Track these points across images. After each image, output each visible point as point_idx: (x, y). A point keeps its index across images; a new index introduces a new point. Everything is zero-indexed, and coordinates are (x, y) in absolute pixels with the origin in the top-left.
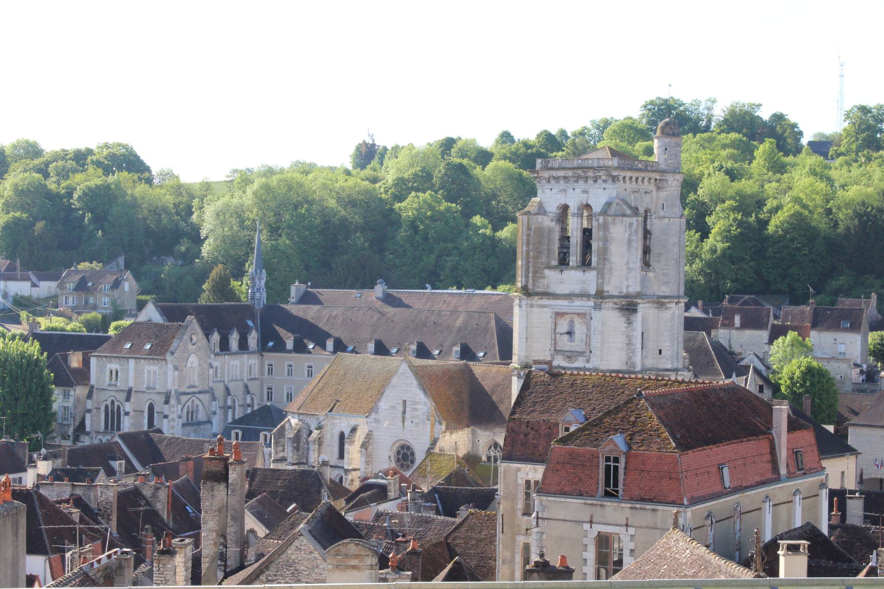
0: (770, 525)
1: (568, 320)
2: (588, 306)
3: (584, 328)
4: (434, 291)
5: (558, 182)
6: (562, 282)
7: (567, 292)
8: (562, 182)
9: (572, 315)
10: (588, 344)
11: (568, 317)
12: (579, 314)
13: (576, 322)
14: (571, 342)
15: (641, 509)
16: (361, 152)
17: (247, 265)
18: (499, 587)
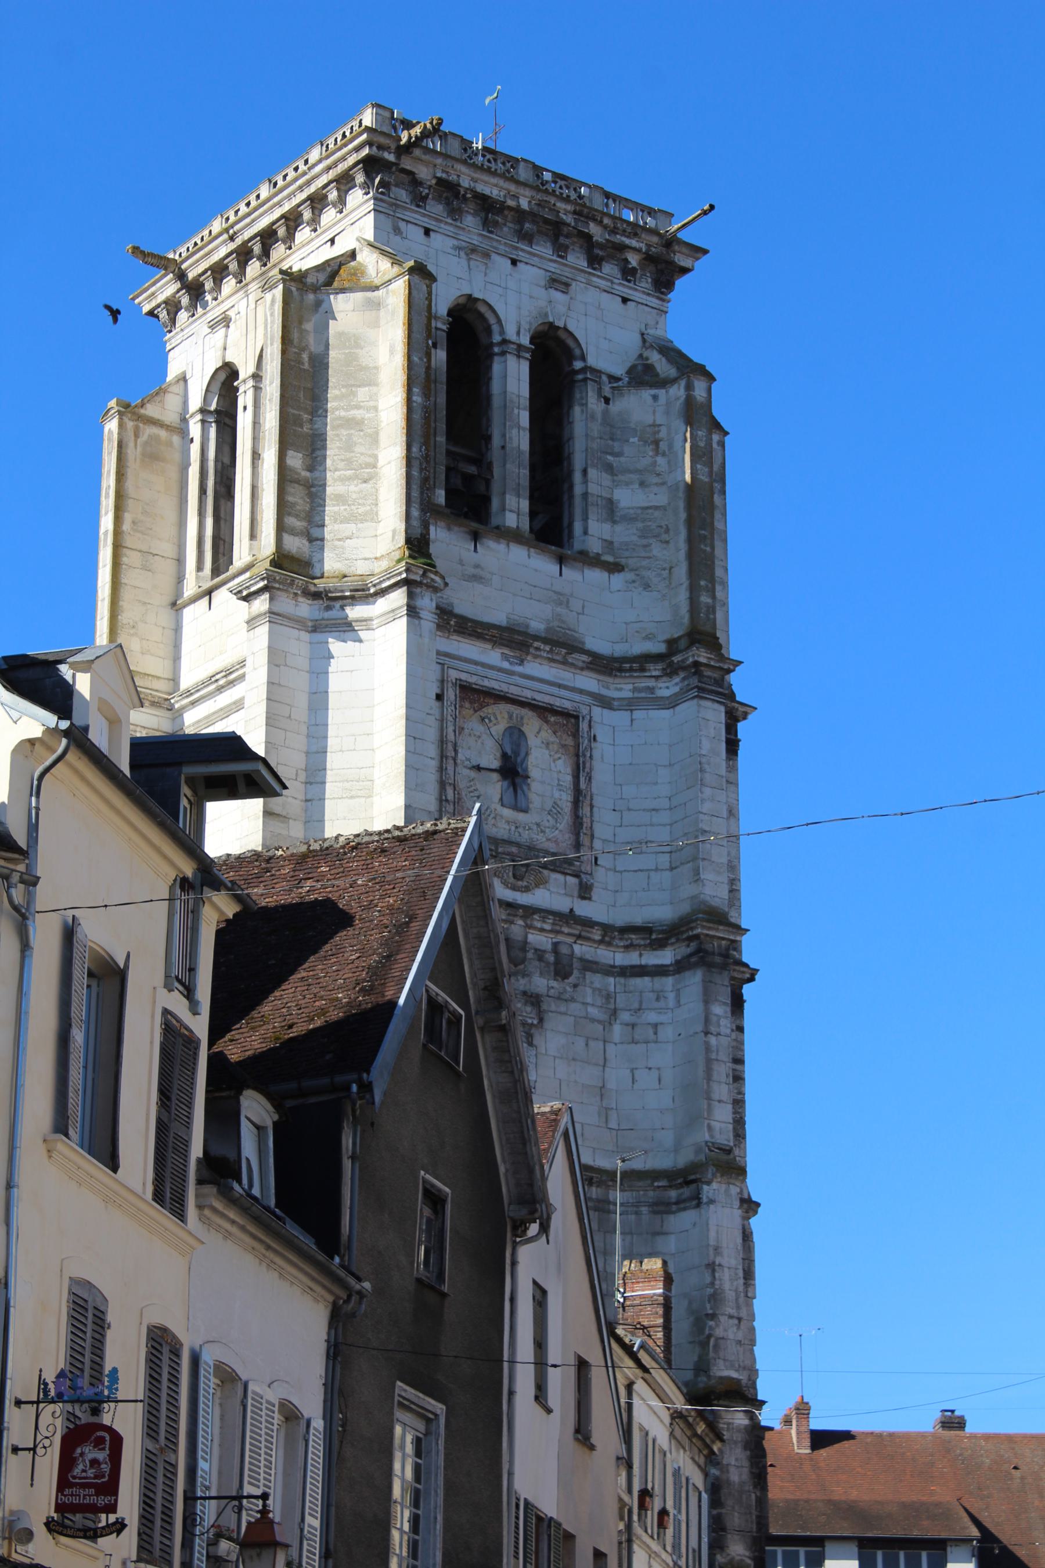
0: (707, 1562)
1: (499, 728)
2: (581, 692)
3: (563, 768)
5: (455, 213)
7: (499, 617)
8: (470, 221)
11: (501, 715)
12: (544, 711)
14: (516, 808)
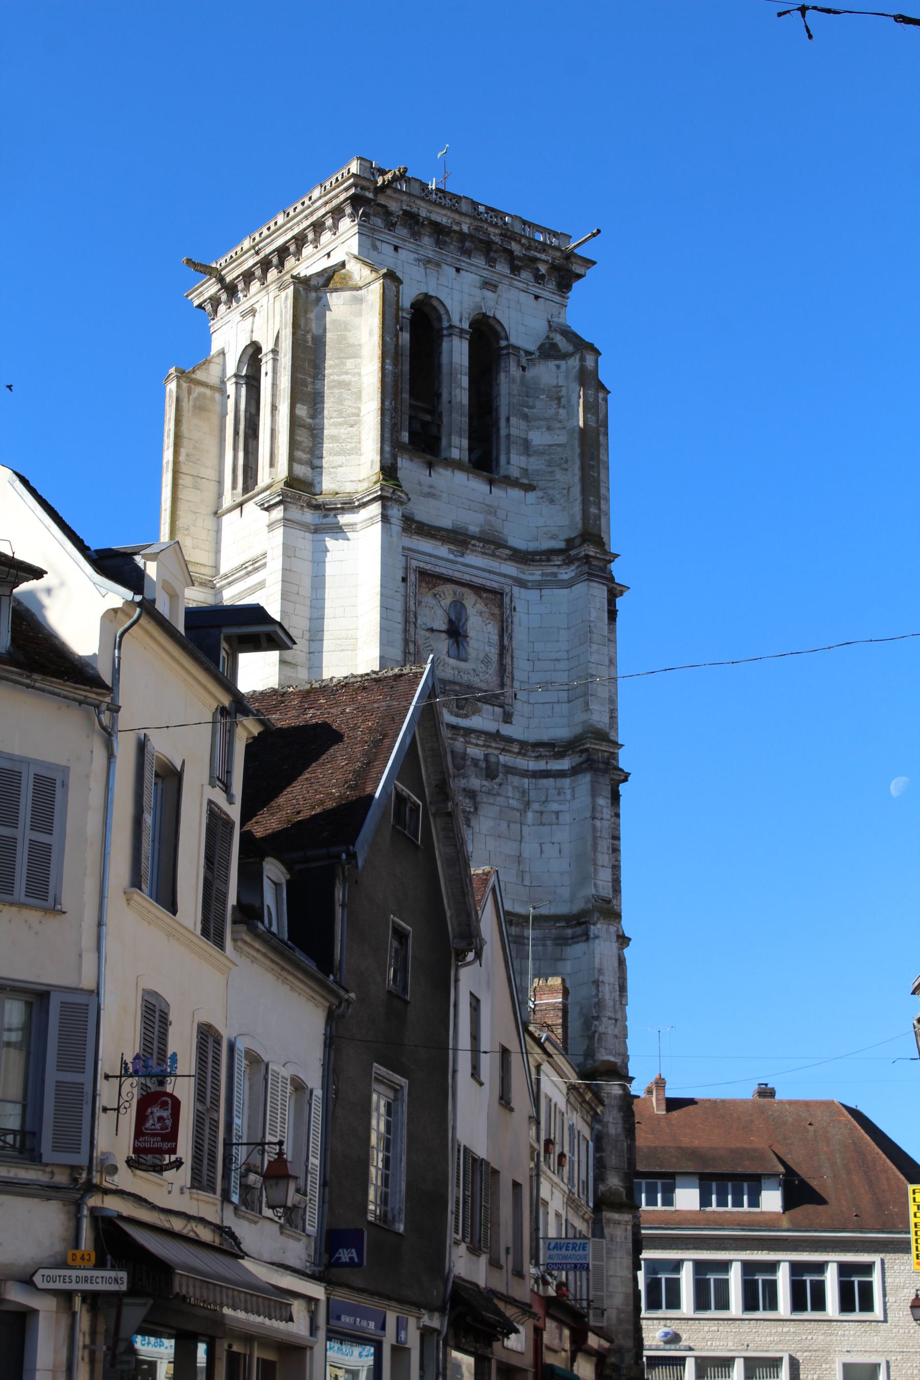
1: (447, 602)
2: (505, 576)
3: (492, 630)
4: (185, 1147)
7: (446, 522)
9: (459, 589)
11: (448, 593)
12: (478, 589)
16: (86, 666)
17: (243, 1170)
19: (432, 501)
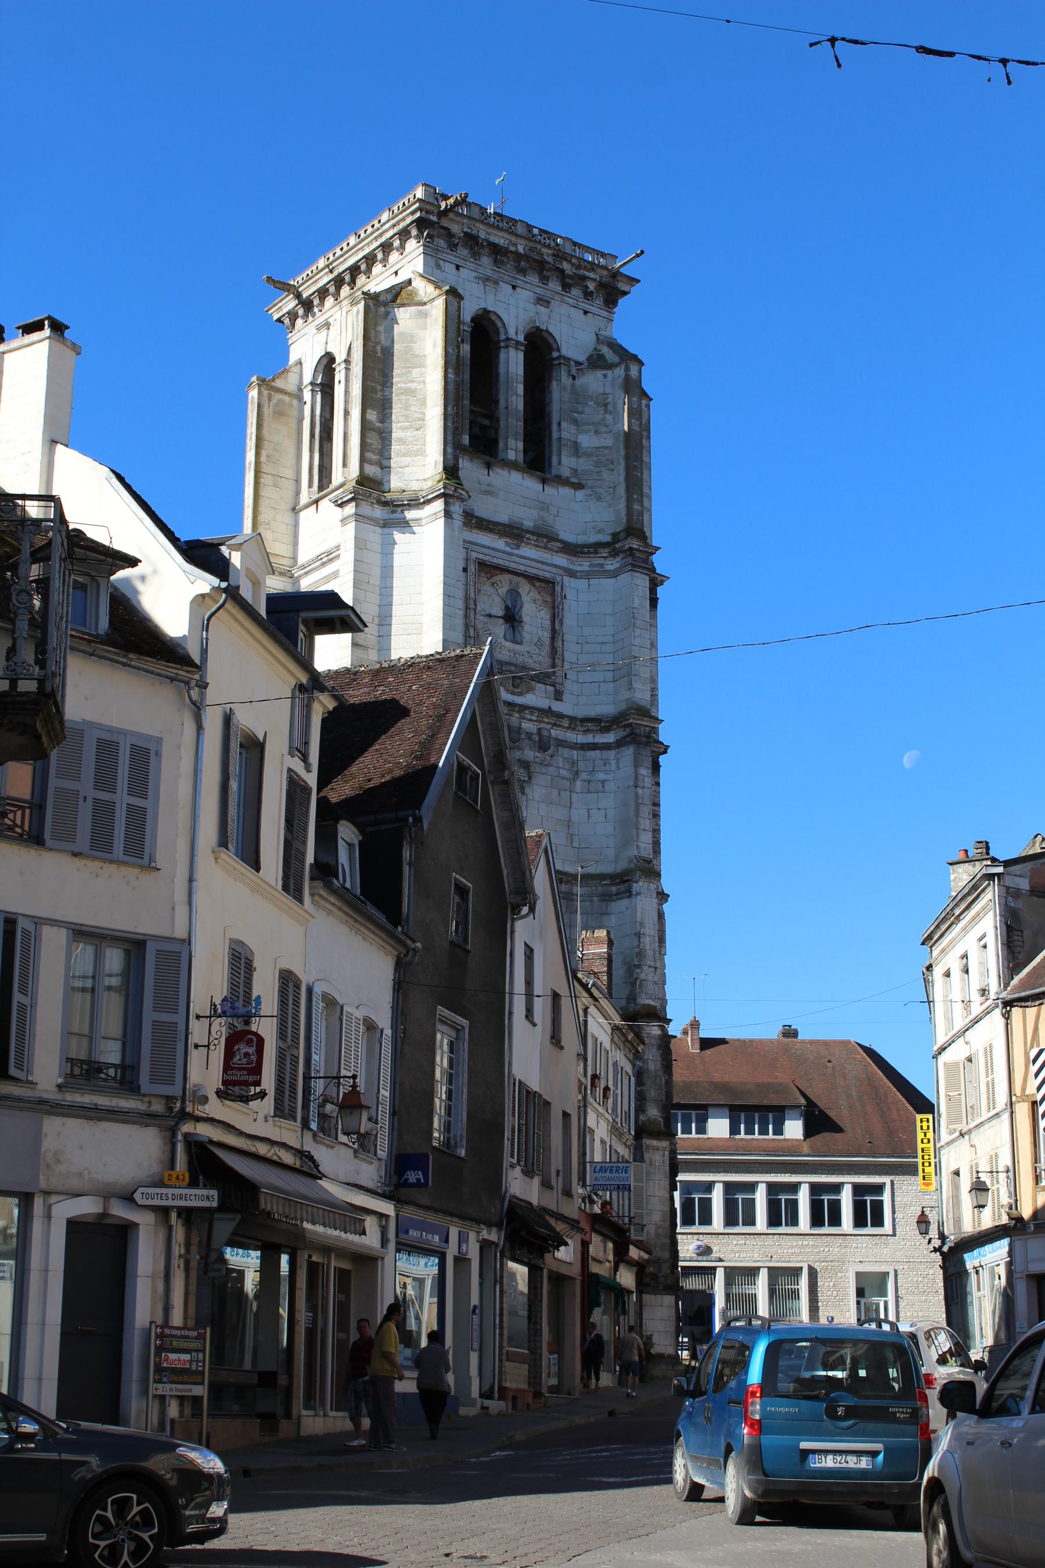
1: (503, 590)
2: (556, 566)
6: (488, 493)
7: (503, 518)
8: (486, 260)
9: (515, 579)
10: (555, 653)
11: (505, 582)
12: (532, 579)
13: (525, 598)
15: (996, 927)
18: (281, 1327)
19: (490, 498)
